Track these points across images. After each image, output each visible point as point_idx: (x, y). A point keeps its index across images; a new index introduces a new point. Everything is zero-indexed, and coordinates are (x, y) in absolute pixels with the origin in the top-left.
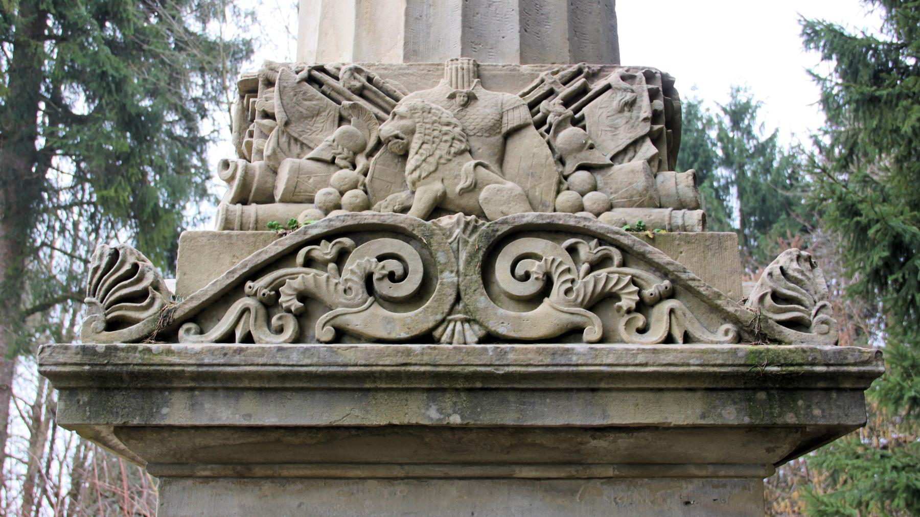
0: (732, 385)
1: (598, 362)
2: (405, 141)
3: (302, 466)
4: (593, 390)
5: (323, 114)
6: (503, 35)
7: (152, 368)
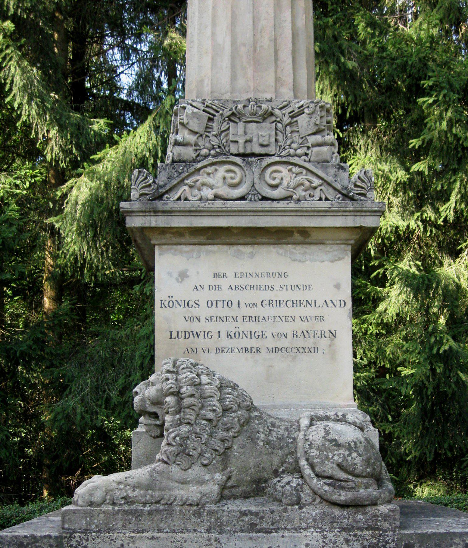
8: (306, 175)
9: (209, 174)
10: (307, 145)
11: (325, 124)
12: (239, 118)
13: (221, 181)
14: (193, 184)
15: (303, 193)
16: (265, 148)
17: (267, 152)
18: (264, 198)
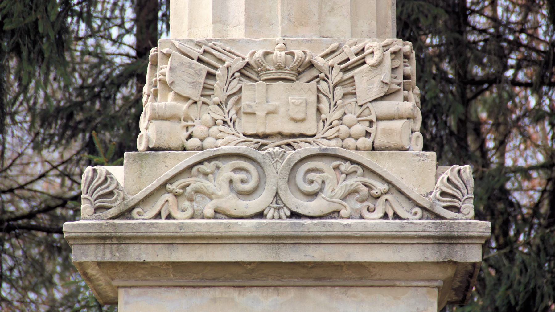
8: (363, 176)
9: (206, 175)
10: (369, 118)
11: (401, 80)
12: (257, 73)
13: (226, 187)
14: (181, 191)
15: (358, 206)
16: (300, 124)
17: (302, 131)
18: (294, 215)
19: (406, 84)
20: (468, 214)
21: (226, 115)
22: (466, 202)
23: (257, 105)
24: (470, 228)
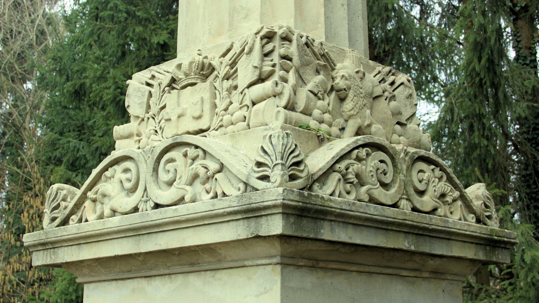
0: (482, 242)
1: (455, 227)
2: (347, 92)
3: (337, 263)
4: (449, 239)
5: (311, 65)
6: (357, 39)
7: (325, 208)
13: (118, 186)
18: (157, 206)
19: (282, 64)
20: (275, 182)
21: (157, 124)
22: (275, 168)
23: (172, 111)
24: (265, 197)
